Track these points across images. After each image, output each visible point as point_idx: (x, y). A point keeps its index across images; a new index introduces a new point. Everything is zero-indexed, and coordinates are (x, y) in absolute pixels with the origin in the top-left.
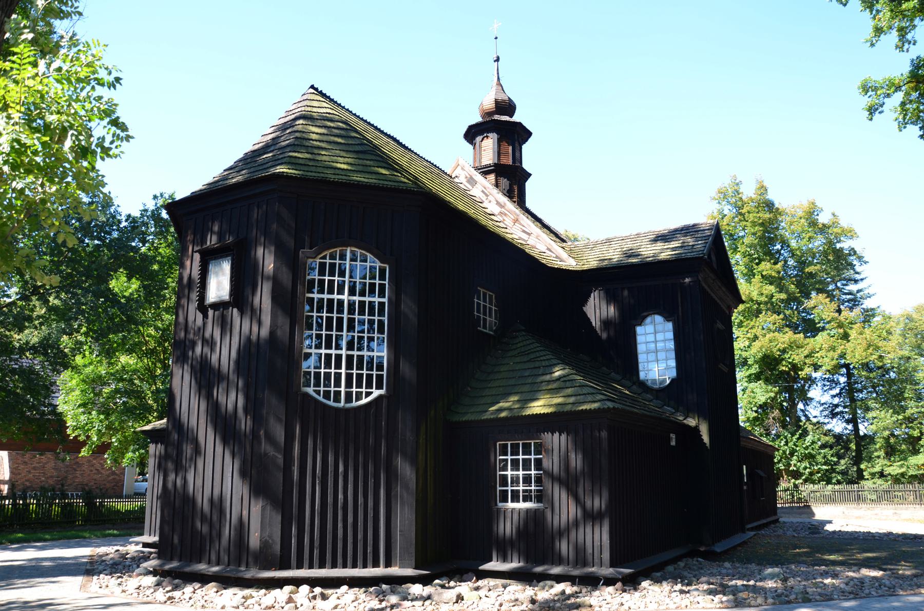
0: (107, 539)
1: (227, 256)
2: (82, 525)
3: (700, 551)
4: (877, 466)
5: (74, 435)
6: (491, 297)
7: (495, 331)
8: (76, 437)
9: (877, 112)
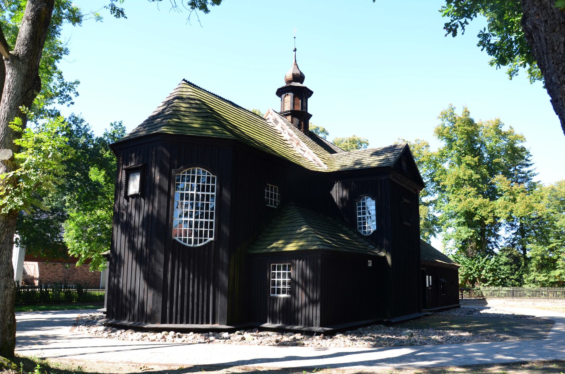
0: (88, 310)
1: (138, 172)
2: (75, 303)
3: (383, 321)
4: (531, 276)
5: (72, 254)
6: (275, 189)
7: (277, 206)
8: (73, 256)
9: (514, 75)
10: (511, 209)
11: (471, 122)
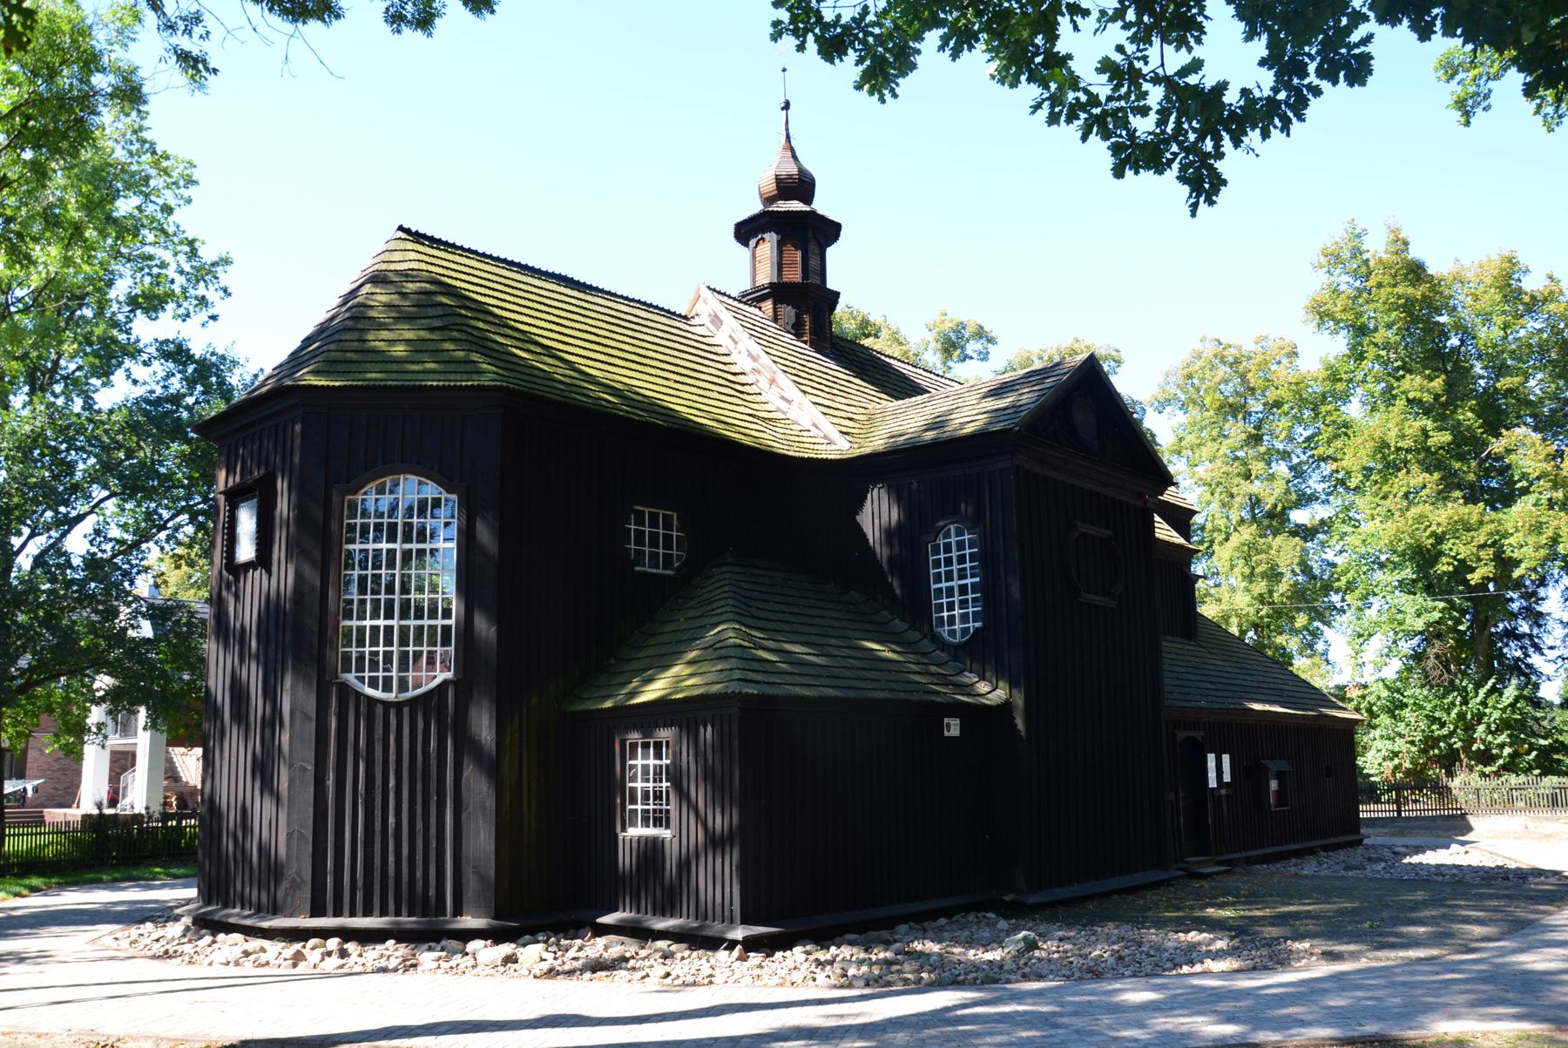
7: (678, 570)
9: (1479, 111)
10: (1555, 533)
11: (1416, 271)
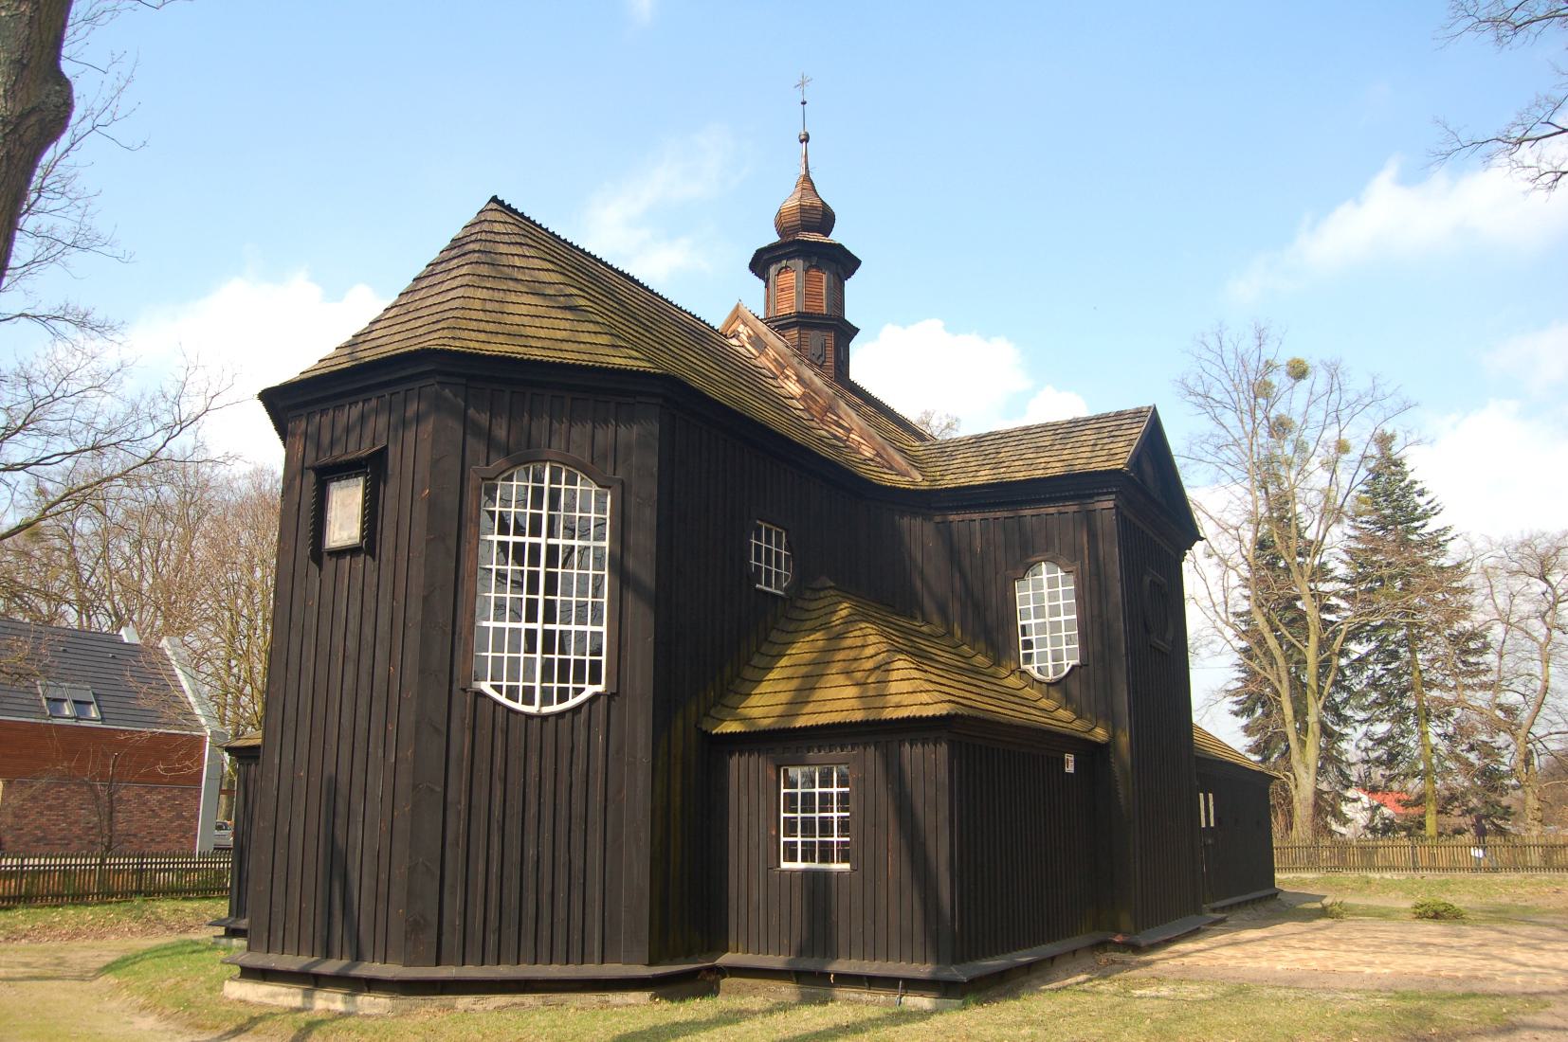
7: (786, 590)
